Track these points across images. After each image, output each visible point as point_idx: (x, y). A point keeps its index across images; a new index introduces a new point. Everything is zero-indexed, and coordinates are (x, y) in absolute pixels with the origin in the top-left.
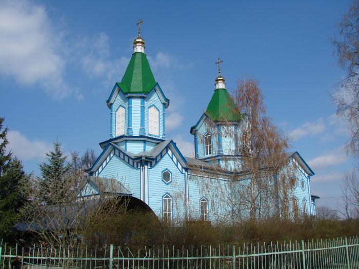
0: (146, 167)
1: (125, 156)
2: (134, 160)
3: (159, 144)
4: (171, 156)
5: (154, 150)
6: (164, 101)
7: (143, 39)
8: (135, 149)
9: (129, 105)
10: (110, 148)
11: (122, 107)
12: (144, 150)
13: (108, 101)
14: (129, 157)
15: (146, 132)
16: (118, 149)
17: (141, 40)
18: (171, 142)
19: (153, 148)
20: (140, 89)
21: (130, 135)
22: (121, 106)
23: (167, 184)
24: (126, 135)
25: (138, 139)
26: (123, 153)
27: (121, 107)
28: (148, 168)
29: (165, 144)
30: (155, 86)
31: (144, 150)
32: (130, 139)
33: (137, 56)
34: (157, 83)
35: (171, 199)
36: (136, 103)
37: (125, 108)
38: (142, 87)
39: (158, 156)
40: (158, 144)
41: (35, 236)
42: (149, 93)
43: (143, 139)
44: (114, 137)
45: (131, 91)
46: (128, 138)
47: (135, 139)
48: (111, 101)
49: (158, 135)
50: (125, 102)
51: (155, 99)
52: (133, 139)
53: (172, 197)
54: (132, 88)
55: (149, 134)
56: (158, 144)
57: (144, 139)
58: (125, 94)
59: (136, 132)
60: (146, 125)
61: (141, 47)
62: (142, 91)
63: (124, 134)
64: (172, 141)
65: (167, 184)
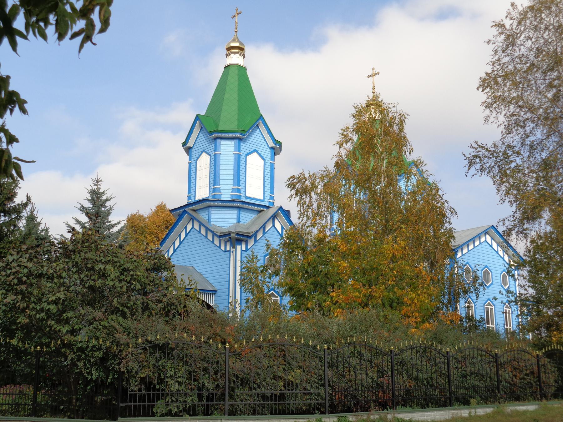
0: (239, 248)
1: (209, 232)
2: (220, 237)
3: (262, 213)
4: (280, 232)
5: (253, 222)
6: (272, 144)
7: (241, 43)
8: (224, 220)
9: (215, 150)
10: (185, 218)
11: (206, 152)
12: (239, 222)
13: (184, 144)
14: (214, 234)
15: (242, 194)
16: (198, 221)
17: (237, 44)
18: (279, 209)
19: (254, 216)
20: (234, 127)
21: (217, 198)
22: (203, 151)
23: (467, 263)
24: (210, 198)
25: (228, 204)
26: (205, 226)
27: (204, 154)
28: (242, 251)
29: (271, 212)
30: (258, 120)
31: (239, 222)
32: (216, 204)
33: (232, 69)
34: (262, 116)
35: (493, 307)
36: (227, 148)
37: (210, 155)
38: (236, 122)
39: (257, 232)
40: (260, 211)
41: (66, 303)
42: (247, 131)
43: (235, 204)
44: (193, 201)
45: (220, 128)
46: (213, 203)
47: (224, 204)
48: (190, 144)
49: (262, 198)
50: (210, 143)
51: (257, 139)
52: (220, 204)
53: (494, 305)
54: (221, 123)
55: (246, 197)
56: (260, 211)
57: (238, 204)
58: (211, 133)
59: (226, 195)
60: (242, 182)
61: (238, 55)
62: (236, 128)
63: (207, 196)
64: (281, 207)
65: (486, 267)
